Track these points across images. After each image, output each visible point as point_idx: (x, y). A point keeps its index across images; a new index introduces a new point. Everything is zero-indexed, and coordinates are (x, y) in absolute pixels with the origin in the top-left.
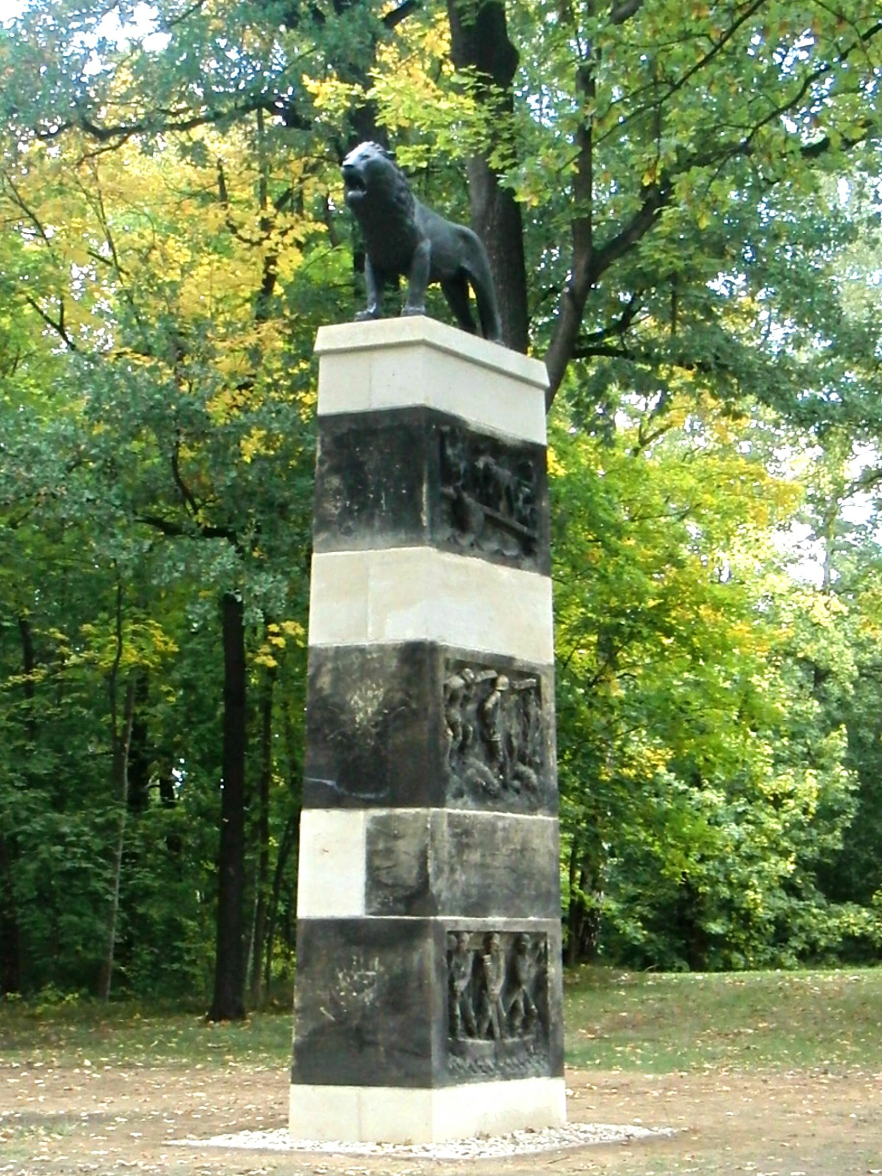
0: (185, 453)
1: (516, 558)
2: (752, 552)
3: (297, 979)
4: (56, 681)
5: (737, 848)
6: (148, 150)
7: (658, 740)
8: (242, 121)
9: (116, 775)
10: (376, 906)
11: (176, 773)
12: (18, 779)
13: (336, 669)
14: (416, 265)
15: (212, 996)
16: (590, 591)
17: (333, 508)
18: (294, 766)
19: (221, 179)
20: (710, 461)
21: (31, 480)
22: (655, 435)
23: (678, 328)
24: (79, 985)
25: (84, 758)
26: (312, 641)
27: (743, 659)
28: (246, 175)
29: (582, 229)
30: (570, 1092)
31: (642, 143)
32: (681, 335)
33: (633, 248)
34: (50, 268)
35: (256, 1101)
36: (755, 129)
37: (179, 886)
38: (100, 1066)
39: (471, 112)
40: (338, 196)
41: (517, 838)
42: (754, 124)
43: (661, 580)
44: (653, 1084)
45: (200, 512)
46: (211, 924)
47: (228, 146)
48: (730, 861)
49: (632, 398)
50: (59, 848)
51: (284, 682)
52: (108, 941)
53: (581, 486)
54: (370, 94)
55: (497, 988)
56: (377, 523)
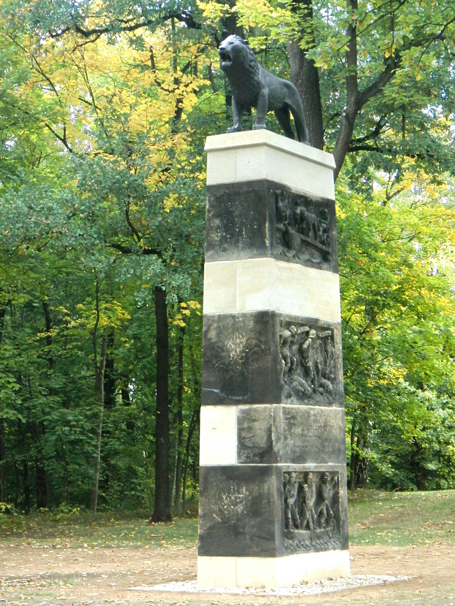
0: (133, 208)
1: (319, 263)
2: (449, 258)
3: (200, 499)
4: (63, 336)
5: (443, 422)
6: (111, 42)
7: (399, 364)
8: (163, 25)
9: (98, 388)
10: (243, 458)
11: (131, 387)
12: (44, 390)
13: (219, 327)
14: (260, 102)
15: (153, 509)
16: (361, 281)
17: (216, 237)
18: (196, 383)
19: (152, 57)
20: (425, 208)
21: (48, 224)
22: (395, 194)
23: (406, 135)
24: (80, 503)
25: (79, 378)
26: (205, 312)
27: (446, 318)
28: (165, 54)
29: (352, 81)
30: (352, 558)
31: (384, 34)
32: (408, 139)
33: (380, 91)
34: (58, 108)
35: (179, 565)
36: (446, 26)
37: (134, 449)
38: (93, 547)
39: (289, 18)
40: (217, 65)
41: (322, 421)
42: (445, 23)
43: (400, 275)
44: (398, 552)
45: (142, 240)
46: (152, 470)
47: (155, 39)
48: (439, 429)
49: (381, 174)
50: (67, 428)
51: (189, 335)
52: (95, 479)
53: (355, 223)
54: (233, 10)
55: (311, 502)
56: (241, 245)
